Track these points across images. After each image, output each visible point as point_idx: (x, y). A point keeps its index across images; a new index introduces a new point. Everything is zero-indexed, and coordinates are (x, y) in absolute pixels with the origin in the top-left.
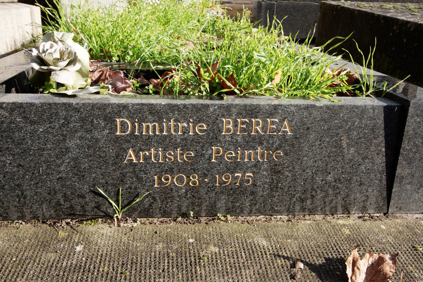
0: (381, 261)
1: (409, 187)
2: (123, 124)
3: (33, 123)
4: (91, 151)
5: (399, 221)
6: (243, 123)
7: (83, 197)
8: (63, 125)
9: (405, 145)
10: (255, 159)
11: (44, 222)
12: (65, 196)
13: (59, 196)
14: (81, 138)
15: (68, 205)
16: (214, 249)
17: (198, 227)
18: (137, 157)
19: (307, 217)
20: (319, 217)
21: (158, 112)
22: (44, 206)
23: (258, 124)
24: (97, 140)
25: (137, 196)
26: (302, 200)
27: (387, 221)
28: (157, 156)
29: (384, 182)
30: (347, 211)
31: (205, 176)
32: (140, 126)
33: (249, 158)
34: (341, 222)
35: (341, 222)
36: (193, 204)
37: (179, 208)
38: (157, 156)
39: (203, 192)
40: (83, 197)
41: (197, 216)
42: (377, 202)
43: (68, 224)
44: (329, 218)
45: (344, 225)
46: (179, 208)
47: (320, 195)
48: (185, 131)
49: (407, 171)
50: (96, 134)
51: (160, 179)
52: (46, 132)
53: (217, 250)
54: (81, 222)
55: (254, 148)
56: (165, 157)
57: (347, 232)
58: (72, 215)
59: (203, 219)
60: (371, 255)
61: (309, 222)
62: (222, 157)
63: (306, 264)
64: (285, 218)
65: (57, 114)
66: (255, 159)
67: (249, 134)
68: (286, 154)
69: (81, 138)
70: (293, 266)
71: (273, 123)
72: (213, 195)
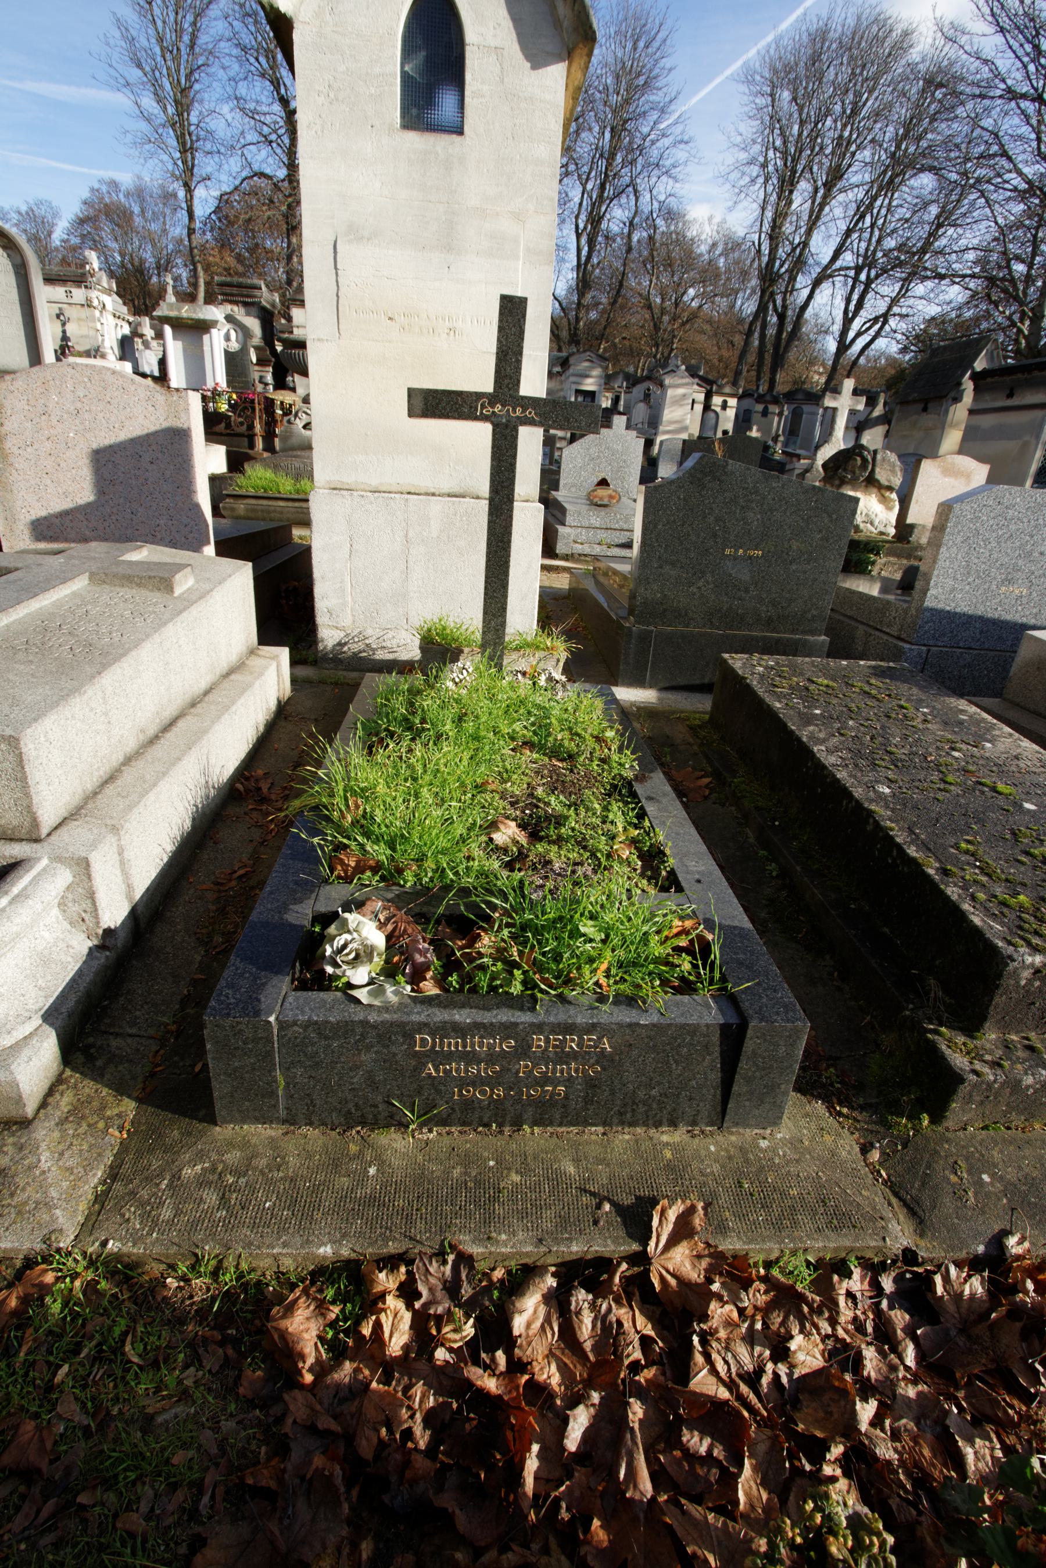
0: (691, 1210)
1: (747, 1103)
2: (423, 1040)
3: (327, 1038)
4: (387, 1065)
5: (733, 1138)
6: (555, 1040)
7: (376, 1106)
8: (359, 1041)
9: (744, 1065)
10: (569, 1073)
11: (332, 1129)
12: (356, 1105)
13: (351, 1105)
14: (376, 1053)
15: (359, 1113)
16: (516, 1178)
17: (499, 1142)
18: (437, 1070)
19: (626, 1130)
20: (639, 1130)
21: (462, 1029)
22: (334, 1115)
23: (573, 1040)
24: (395, 1055)
25: (435, 1107)
26: (621, 1114)
27: (720, 1138)
28: (458, 1070)
29: (719, 1097)
30: (673, 1124)
31: (511, 1089)
32: (442, 1041)
33: (562, 1072)
34: (665, 1138)
35: (665, 1138)
36: (496, 1115)
37: (481, 1118)
38: (458, 1070)
39: (508, 1104)
40: (376, 1106)
41: (500, 1125)
42: (709, 1116)
43: (358, 1132)
44: (652, 1131)
45: (667, 1144)
46: (481, 1118)
47: (642, 1109)
48: (490, 1047)
49: (745, 1089)
50: (393, 1049)
51: (460, 1091)
52: (341, 1046)
53: (519, 1178)
54: (372, 1130)
55: (568, 1064)
56: (467, 1071)
57: (668, 1154)
58: (363, 1123)
59: (507, 1130)
60: (683, 1202)
61: (627, 1137)
62: (531, 1071)
63: (613, 1204)
64: (600, 1129)
65: (353, 1030)
66: (569, 1073)
67: (563, 1051)
68: (604, 1069)
69: (376, 1053)
70: (599, 1206)
71: (590, 1040)
72: (519, 1107)
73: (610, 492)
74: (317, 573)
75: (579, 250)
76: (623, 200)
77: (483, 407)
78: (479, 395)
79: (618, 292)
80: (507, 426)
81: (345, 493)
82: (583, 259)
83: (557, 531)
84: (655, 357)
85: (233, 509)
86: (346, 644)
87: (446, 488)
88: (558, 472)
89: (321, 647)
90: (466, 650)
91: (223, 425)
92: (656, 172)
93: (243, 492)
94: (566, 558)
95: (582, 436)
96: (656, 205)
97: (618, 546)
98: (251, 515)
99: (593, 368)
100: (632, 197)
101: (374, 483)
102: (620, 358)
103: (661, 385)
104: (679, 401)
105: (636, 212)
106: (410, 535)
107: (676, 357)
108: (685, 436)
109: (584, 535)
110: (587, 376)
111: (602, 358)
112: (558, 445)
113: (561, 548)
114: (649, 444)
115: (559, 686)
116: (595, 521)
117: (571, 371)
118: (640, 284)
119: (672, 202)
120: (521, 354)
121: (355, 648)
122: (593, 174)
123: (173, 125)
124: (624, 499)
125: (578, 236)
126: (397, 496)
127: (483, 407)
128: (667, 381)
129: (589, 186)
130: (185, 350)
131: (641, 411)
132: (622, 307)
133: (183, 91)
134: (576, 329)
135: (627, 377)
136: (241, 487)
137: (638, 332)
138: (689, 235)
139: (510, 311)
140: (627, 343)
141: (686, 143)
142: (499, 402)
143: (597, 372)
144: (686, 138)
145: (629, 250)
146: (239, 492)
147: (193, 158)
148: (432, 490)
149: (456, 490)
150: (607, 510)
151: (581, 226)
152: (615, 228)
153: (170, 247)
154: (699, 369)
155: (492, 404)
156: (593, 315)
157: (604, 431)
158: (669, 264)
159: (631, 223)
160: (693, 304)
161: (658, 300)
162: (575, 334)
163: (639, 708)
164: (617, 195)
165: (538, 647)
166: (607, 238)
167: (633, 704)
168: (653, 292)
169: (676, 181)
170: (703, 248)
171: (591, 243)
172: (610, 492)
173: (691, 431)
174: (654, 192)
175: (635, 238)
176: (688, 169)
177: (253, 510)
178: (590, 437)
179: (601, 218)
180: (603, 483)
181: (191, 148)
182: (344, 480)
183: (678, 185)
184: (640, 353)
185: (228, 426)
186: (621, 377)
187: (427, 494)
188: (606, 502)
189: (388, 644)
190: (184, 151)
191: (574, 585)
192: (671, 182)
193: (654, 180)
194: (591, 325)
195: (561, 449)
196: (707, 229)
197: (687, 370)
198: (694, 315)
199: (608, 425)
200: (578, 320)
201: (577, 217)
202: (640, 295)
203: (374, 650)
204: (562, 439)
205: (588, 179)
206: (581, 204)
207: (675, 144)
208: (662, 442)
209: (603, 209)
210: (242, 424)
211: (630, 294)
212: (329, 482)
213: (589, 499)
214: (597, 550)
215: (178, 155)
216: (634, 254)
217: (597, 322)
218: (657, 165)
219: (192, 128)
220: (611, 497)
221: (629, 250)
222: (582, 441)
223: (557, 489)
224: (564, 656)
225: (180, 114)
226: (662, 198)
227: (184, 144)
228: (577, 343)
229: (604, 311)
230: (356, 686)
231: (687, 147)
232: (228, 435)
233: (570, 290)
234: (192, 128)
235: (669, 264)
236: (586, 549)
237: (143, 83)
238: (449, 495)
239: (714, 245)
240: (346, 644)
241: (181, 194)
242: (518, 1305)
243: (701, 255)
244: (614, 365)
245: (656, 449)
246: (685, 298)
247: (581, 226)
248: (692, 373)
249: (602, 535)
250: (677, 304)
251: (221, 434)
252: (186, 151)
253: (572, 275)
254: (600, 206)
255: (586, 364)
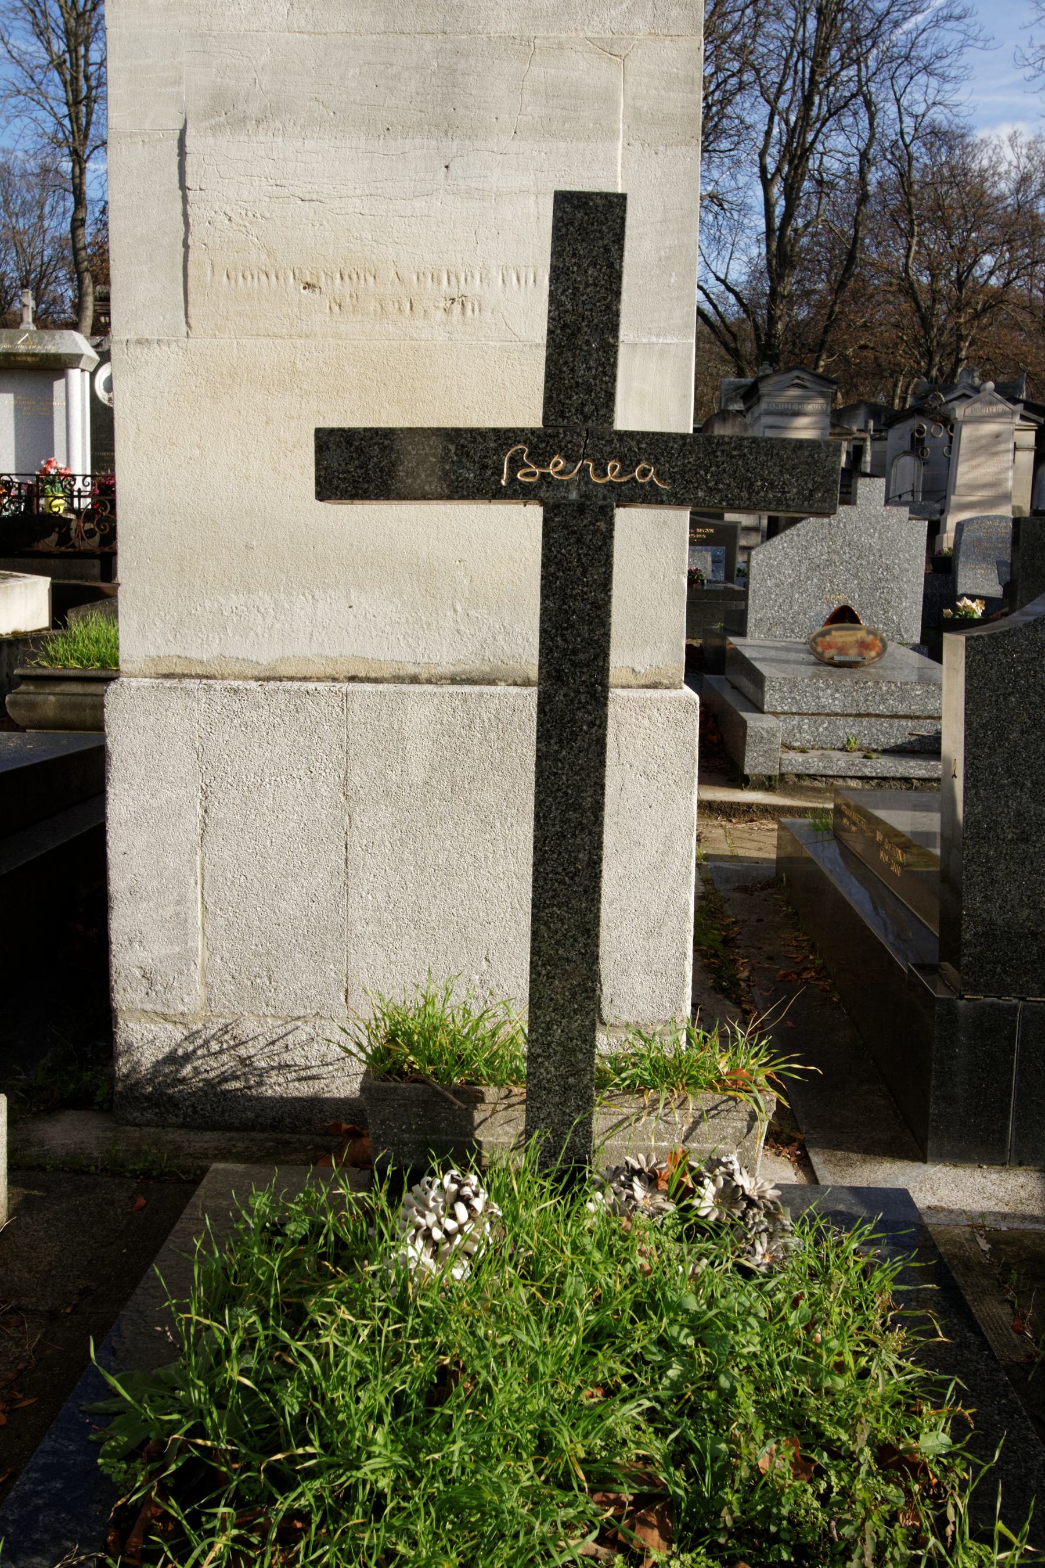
73: (861, 634)
74: (118, 881)
75: (769, 206)
76: (848, 120)
77: (516, 464)
78: (505, 437)
79: (847, 269)
80: (581, 508)
81: (191, 684)
82: (777, 222)
83: (743, 724)
84: (927, 374)
85: (32, 706)
86: (187, 1057)
87: (446, 660)
88: (744, 596)
89: (123, 1066)
90: (491, 1093)
91: (54, 537)
92: (905, 69)
93: (57, 669)
94: (767, 784)
95: (793, 522)
96: (908, 121)
97: (885, 752)
98: (71, 716)
99: (807, 398)
100: (863, 114)
101: (266, 657)
102: (858, 380)
103: (949, 423)
104: (990, 447)
105: (872, 137)
106: (355, 780)
107: (970, 372)
108: (1006, 511)
109: (806, 731)
110: (797, 414)
111: (824, 379)
112: (743, 542)
113: (754, 763)
114: (935, 530)
115: (757, 1216)
116: (832, 700)
117: (763, 405)
118: (887, 254)
119: (939, 116)
120: (614, 328)
121: (212, 1068)
122: (789, 84)
123: (59, 67)
124: (892, 646)
125: (767, 184)
126: (320, 686)
127: (516, 464)
128: (960, 412)
129: (783, 102)
130: (18, 409)
131: (907, 468)
132: (855, 296)
133: (80, 16)
134: (769, 336)
135: (874, 412)
136: (52, 660)
137: (890, 334)
138: (975, 166)
139: (581, 229)
140: (870, 354)
141: (959, 18)
142: (561, 449)
143: (816, 405)
144: (957, 12)
145: (864, 198)
146: (50, 669)
147: (89, 114)
148: (411, 670)
149: (473, 665)
150: (857, 673)
151: (771, 167)
152: (833, 164)
153: (48, 252)
154: (1018, 389)
155: (540, 457)
156: (802, 313)
157: (841, 509)
158: (940, 218)
159: (864, 156)
160: (993, 281)
161: (925, 280)
162: (769, 345)
163: (996, 1239)
164: (834, 112)
165: (693, 1082)
166: (820, 183)
167: (977, 1223)
168: (913, 267)
169: (944, 78)
170: (1004, 187)
171: (791, 193)
172: (861, 634)
173: (1015, 502)
174: (905, 102)
175: (874, 177)
176: (964, 60)
177: (74, 707)
178: (812, 523)
179: (807, 151)
180: (844, 616)
181: (87, 97)
182: (193, 654)
183: (948, 86)
184: (896, 370)
185: (64, 538)
186: (862, 412)
187: (398, 679)
188: (852, 655)
189: (297, 1057)
190: (74, 103)
191: (789, 849)
192: (934, 82)
193: (902, 82)
194: (795, 330)
195: (748, 549)
196: (1008, 154)
197: (998, 389)
198: (997, 299)
199: (848, 498)
200: (772, 320)
201: (762, 155)
202: (891, 272)
203: (262, 1073)
204: (748, 530)
205: (780, 92)
206: (768, 133)
207: (936, 23)
208: (960, 527)
209: (810, 137)
210: (91, 533)
211: (867, 273)
212: (156, 660)
213: (813, 651)
214: (840, 762)
215: (65, 110)
216: (873, 206)
217: (807, 322)
218: (907, 58)
219: (92, 69)
220: (863, 645)
221: (864, 198)
222: (792, 531)
223: (742, 633)
224: (768, 1101)
225: (72, 50)
226: (920, 109)
227: (76, 92)
228: (774, 360)
229: (821, 305)
230: (204, 1171)
231: (961, 26)
232: (62, 556)
233: (755, 275)
234: (92, 69)
235: (940, 218)
236: (814, 762)
237: (14, 10)
238: (454, 680)
239: (1025, 180)
240: (187, 1057)
241: (67, 166)
242: (785, 1151)
243: (1001, 198)
244: (846, 395)
245: (948, 540)
246: (977, 272)
247: (771, 167)
248: (1008, 393)
249: (847, 729)
250: (960, 283)
251: (49, 555)
252: (77, 103)
253: (757, 251)
254: (804, 133)
255: (794, 392)
